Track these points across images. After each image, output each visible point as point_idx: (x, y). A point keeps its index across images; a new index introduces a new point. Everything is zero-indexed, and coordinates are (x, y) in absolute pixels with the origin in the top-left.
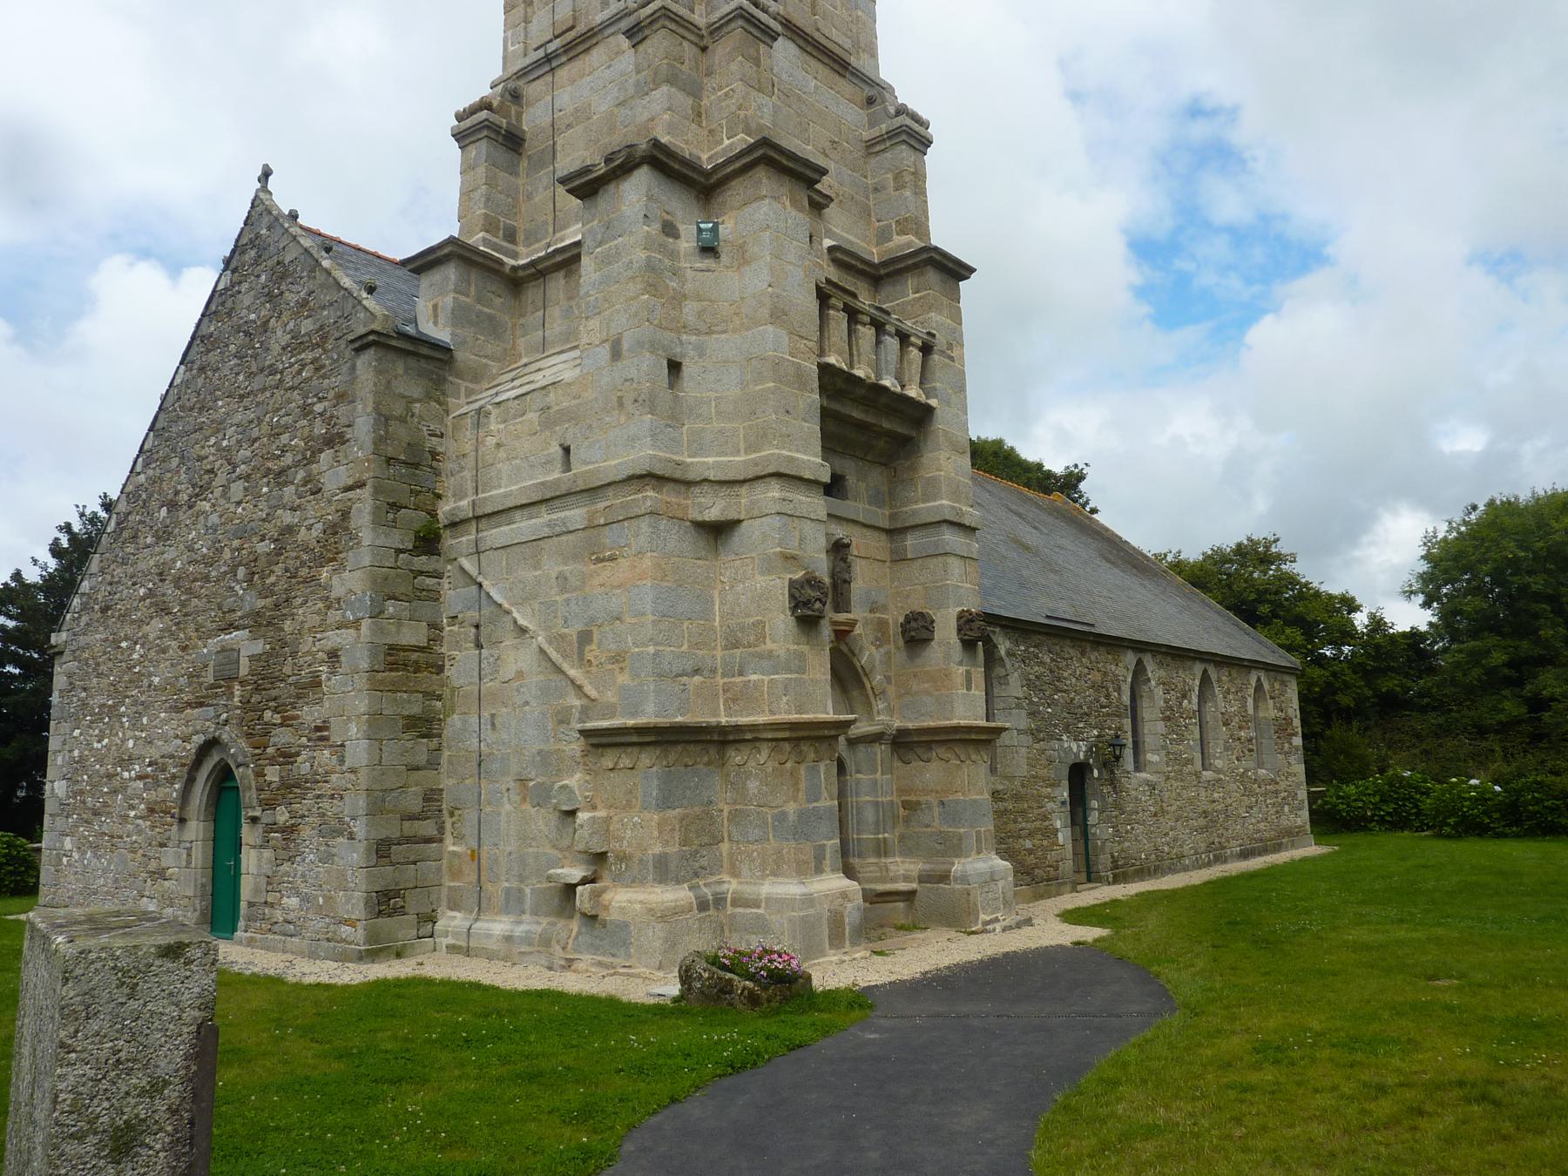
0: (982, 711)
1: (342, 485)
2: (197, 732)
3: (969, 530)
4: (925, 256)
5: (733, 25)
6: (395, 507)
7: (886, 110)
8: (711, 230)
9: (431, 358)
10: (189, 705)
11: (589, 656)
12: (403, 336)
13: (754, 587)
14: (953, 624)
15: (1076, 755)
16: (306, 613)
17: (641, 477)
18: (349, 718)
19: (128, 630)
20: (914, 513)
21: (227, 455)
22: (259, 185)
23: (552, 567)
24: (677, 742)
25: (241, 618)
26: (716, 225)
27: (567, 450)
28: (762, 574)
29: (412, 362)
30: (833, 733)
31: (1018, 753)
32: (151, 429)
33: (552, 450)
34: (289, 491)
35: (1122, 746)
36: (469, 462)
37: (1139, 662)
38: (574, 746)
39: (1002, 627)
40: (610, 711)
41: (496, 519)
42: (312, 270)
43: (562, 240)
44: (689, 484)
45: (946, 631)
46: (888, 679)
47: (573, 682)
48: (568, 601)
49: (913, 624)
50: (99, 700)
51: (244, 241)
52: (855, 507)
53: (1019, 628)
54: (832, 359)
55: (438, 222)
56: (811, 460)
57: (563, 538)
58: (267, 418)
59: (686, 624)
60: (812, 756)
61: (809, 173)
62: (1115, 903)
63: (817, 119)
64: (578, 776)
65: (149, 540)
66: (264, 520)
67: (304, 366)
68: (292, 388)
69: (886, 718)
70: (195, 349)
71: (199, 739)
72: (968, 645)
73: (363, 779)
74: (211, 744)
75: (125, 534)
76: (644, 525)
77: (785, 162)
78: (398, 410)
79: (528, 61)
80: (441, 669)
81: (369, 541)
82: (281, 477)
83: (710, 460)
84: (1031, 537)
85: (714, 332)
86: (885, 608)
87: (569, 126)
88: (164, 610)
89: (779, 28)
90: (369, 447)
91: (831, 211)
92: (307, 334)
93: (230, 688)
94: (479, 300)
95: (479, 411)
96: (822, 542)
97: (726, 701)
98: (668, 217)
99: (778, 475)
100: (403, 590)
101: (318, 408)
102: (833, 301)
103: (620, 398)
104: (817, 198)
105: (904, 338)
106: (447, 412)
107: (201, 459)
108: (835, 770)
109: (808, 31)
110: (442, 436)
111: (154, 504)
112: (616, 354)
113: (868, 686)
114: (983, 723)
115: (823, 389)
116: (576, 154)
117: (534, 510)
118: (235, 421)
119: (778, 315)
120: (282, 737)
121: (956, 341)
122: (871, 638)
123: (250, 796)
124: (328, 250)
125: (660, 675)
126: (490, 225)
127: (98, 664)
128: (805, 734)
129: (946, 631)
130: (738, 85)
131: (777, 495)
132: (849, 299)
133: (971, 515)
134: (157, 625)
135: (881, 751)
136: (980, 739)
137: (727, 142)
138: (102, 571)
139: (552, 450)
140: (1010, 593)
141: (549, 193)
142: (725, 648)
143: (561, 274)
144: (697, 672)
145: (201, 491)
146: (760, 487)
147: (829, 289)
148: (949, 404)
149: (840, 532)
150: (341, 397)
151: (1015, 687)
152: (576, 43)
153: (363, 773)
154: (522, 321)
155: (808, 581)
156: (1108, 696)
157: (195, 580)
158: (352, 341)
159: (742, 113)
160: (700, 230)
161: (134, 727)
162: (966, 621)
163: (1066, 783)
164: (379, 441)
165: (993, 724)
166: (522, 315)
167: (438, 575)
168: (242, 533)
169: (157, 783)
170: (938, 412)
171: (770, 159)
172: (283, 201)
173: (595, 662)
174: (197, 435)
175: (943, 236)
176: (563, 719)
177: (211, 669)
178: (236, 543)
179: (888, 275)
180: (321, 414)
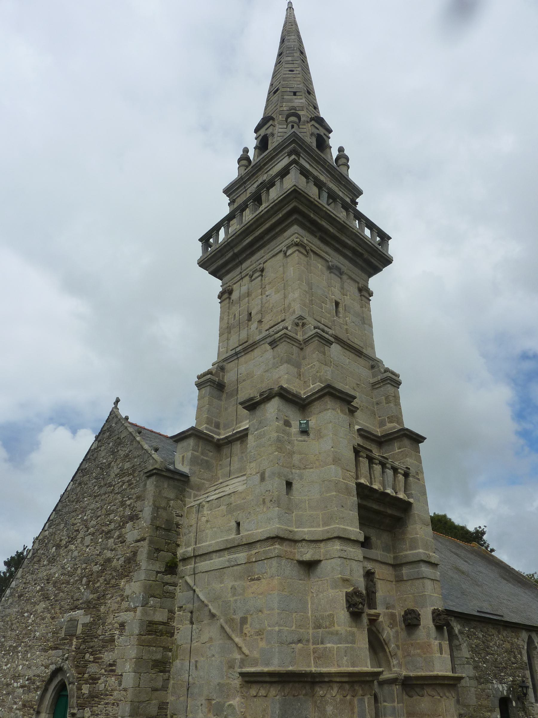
0: (450, 667)
1: (135, 539)
2: (52, 664)
3: (434, 565)
4: (402, 433)
5: (314, 339)
6: (158, 550)
7: (380, 371)
8: (305, 423)
9: (179, 481)
10: (51, 648)
11: (245, 631)
12: (168, 470)
13: (328, 597)
14: (430, 617)
15: (502, 692)
16: (112, 603)
17: (273, 538)
18: (126, 660)
19: (29, 607)
20: (406, 556)
21: (85, 523)
22: (114, 406)
23: (229, 583)
24: (289, 682)
25: (81, 604)
26: (308, 421)
27: (238, 524)
28: (332, 588)
30: (371, 679)
31: (471, 691)
32: (54, 511)
33: (231, 524)
34: (111, 541)
35: (527, 687)
36: (193, 529)
37: (530, 638)
38: (236, 681)
39: (455, 617)
40: (255, 663)
41: (204, 557)
42: (132, 441)
43: (240, 428)
44: (296, 541)
46: (398, 646)
47: (237, 645)
48: (236, 601)
49: (409, 616)
50: (10, 643)
51: (105, 429)
52: (377, 553)
53: (465, 618)
54: (362, 481)
55: (188, 421)
56: (354, 530)
57: (235, 568)
58: (105, 507)
59: (294, 614)
60: (360, 692)
61: (348, 398)
63: (349, 375)
64: (238, 699)
65: (45, 563)
66: (98, 555)
67: (124, 483)
68: (118, 493)
69: (397, 669)
70: (78, 475)
71: (53, 667)
72: (439, 628)
73: (130, 695)
74: (59, 670)
75: (35, 560)
76: (274, 562)
77: (337, 394)
78: (163, 504)
79: (228, 355)
80: (172, 635)
81: (145, 568)
82: (108, 535)
83: (306, 530)
84: (464, 566)
85: (307, 468)
86: (393, 607)
87: (244, 380)
88: (46, 598)
89: (333, 340)
90: (149, 521)
91: (358, 414)
92: (127, 469)
93: (71, 640)
94: (202, 454)
95: (199, 505)
96: (362, 572)
97: (314, 658)
98: (286, 418)
99: (339, 538)
100: (158, 592)
101: (128, 502)
102: (361, 454)
103: (264, 499)
104: (352, 408)
105: (395, 470)
106: (185, 505)
107: (74, 525)
108: (373, 701)
109: (345, 340)
110: (182, 516)
111: (50, 545)
112: (263, 479)
113: (387, 650)
114: (450, 674)
115: (358, 494)
116: (247, 392)
117: (222, 553)
118: (91, 507)
119: (336, 461)
120: (93, 668)
121: (420, 471)
123: (73, 701)
124: (140, 433)
125: (281, 643)
126: (209, 421)
127: (12, 624)
128: (356, 679)
130: (316, 363)
131: (338, 548)
132: (368, 453)
133: (435, 557)
134: (43, 605)
135: (396, 689)
136: (449, 684)
137: (312, 386)
138: (22, 577)
139: (231, 524)
140: (457, 598)
141: (235, 408)
142: (314, 628)
143: (239, 442)
144: (300, 641)
145: (72, 540)
146: (330, 543)
147: (359, 449)
148: (419, 501)
149: (369, 566)
150: (139, 498)
151: (465, 652)
152: (248, 347)
153: (130, 691)
154: (220, 463)
155: (355, 593)
156: (515, 657)
157: (63, 583)
158: (146, 473)
159: (318, 374)
160: (300, 424)
161: (23, 658)
162: (437, 615)
163: (498, 710)
164: (154, 519)
165: (456, 675)
166: (221, 460)
167: (175, 585)
168: (87, 561)
169: (29, 691)
170: (414, 505)
171: (330, 393)
172: (123, 412)
173: (248, 635)
174: (74, 514)
175: (409, 423)
176: (231, 666)
177: (64, 630)
178: (84, 566)
179: (386, 441)
180: (129, 505)
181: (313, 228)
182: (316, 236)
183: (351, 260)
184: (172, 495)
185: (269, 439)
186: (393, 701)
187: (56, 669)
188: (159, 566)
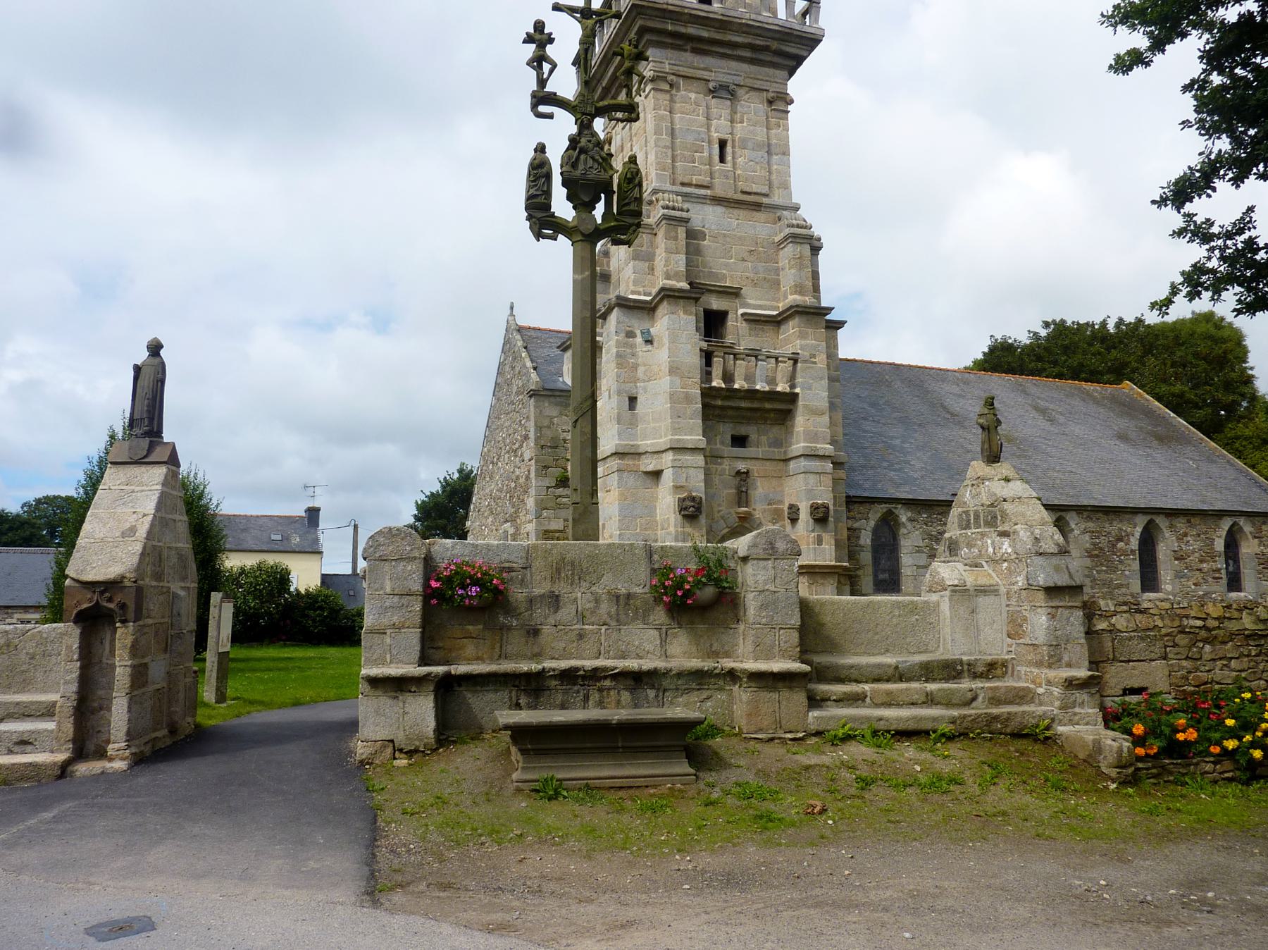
6: (546, 467)
29: (552, 399)
44: (640, 454)
45: (804, 515)
56: (695, 437)
62: (947, 680)
78: (546, 423)
99: (671, 449)
129: (804, 515)
181: (679, 42)
182: (686, 51)
183: (752, 61)
184: (555, 413)
187: (18, 515)
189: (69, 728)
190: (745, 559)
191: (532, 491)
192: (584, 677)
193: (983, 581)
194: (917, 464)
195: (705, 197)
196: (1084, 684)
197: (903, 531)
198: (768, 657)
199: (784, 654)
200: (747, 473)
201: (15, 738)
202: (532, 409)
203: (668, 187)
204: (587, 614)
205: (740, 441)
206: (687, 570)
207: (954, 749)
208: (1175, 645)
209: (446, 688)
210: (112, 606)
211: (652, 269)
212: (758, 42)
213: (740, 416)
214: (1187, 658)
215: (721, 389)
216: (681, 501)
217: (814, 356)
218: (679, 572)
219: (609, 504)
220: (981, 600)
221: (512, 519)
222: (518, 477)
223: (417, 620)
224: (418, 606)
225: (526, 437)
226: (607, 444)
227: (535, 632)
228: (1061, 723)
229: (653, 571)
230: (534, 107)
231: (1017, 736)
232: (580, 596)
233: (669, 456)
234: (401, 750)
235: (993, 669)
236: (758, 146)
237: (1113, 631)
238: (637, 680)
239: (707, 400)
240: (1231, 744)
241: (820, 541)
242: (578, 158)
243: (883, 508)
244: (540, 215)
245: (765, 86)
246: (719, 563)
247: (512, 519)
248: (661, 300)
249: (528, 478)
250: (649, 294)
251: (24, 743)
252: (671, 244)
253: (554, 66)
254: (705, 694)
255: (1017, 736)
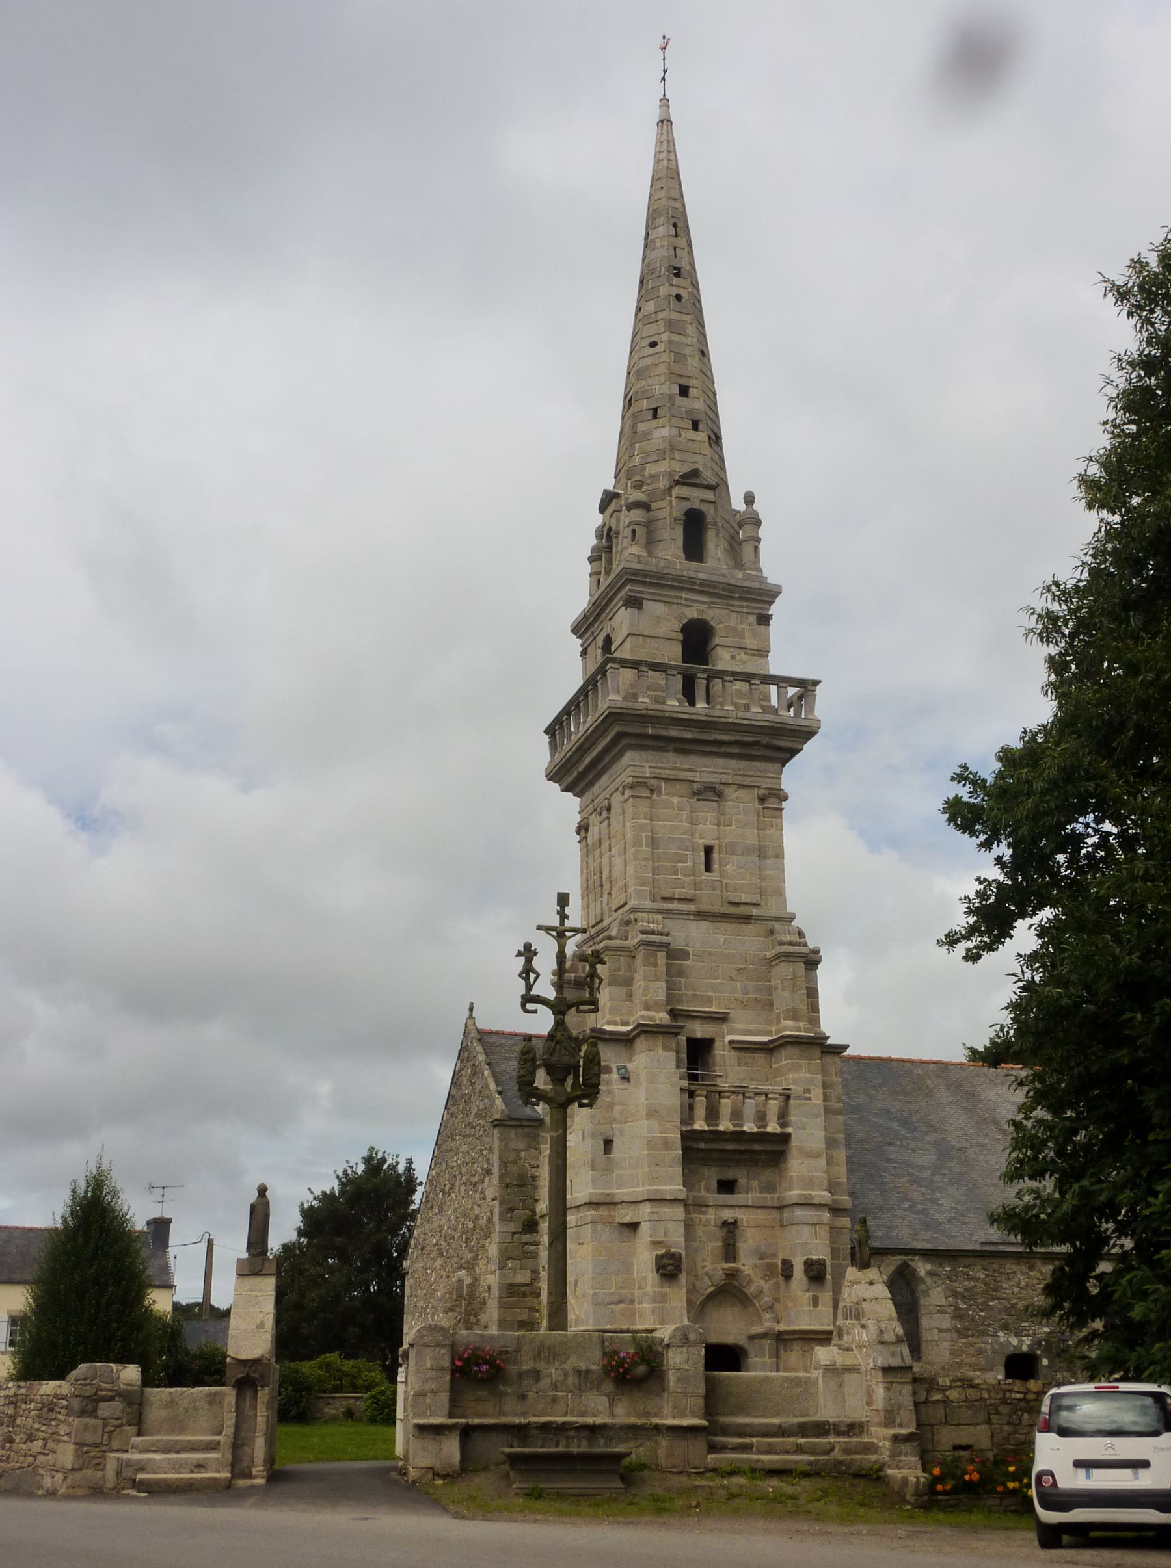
6: (512, 1210)
29: (520, 1130)
44: (616, 1203)
56: (674, 1187)
62: (818, 1436)
78: (512, 1157)
122: (760, 1275)
144: (621, 1302)
182: (668, 751)
184: (521, 1146)
185: (160, 1400)
186: (764, 1356)
188: (513, 1227)
189: (229, 1456)
190: (668, 1346)
191: (496, 1237)
192: (556, 1429)
193: (849, 1361)
194: (946, 1203)
195: (688, 913)
196: (908, 1438)
197: (922, 1287)
198: (683, 1416)
199: (693, 1414)
200: (735, 1223)
201: (195, 1463)
202: (496, 1141)
203: (647, 904)
204: (559, 1384)
205: (727, 1186)
206: (628, 1353)
207: (805, 1483)
208: (997, 1413)
209: (467, 1432)
210: (256, 1375)
211: (630, 995)
212: (746, 739)
213: (728, 1157)
214: (1008, 1424)
215: (704, 1131)
216: (659, 1258)
217: (808, 1091)
218: (622, 1355)
219: (582, 1257)
220: (847, 1377)
221: (470, 1266)
222: (477, 1217)
223: (448, 1387)
224: (448, 1378)
225: (488, 1172)
226: (580, 1188)
227: (523, 1397)
228: (890, 1467)
229: (605, 1354)
230: (523, 1006)
231: (857, 1475)
232: (553, 1372)
233: (647, 1209)
234: (438, 1475)
235: (853, 1428)
236: (747, 851)
237: (946, 1402)
238: (593, 1430)
239: (688, 1144)
240: (1011, 1485)
241: (815, 1302)
242: (554, 1049)
243: (898, 1259)
244: (528, 1089)
245: (756, 782)
246: (650, 1347)
247: (470, 1266)
248: (638, 1035)
249: (490, 1220)
250: (627, 1024)
251: (200, 1466)
252: (649, 970)
253: (538, 975)
254: (639, 1442)
255: (857, 1475)
